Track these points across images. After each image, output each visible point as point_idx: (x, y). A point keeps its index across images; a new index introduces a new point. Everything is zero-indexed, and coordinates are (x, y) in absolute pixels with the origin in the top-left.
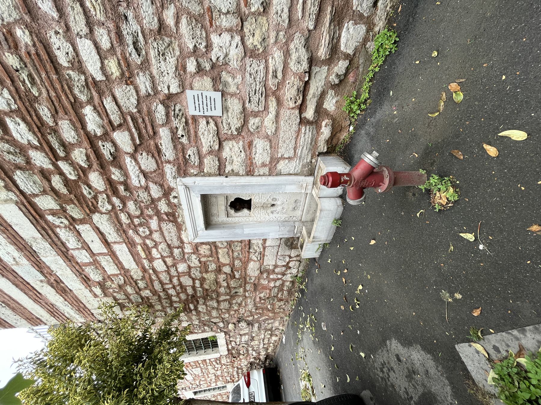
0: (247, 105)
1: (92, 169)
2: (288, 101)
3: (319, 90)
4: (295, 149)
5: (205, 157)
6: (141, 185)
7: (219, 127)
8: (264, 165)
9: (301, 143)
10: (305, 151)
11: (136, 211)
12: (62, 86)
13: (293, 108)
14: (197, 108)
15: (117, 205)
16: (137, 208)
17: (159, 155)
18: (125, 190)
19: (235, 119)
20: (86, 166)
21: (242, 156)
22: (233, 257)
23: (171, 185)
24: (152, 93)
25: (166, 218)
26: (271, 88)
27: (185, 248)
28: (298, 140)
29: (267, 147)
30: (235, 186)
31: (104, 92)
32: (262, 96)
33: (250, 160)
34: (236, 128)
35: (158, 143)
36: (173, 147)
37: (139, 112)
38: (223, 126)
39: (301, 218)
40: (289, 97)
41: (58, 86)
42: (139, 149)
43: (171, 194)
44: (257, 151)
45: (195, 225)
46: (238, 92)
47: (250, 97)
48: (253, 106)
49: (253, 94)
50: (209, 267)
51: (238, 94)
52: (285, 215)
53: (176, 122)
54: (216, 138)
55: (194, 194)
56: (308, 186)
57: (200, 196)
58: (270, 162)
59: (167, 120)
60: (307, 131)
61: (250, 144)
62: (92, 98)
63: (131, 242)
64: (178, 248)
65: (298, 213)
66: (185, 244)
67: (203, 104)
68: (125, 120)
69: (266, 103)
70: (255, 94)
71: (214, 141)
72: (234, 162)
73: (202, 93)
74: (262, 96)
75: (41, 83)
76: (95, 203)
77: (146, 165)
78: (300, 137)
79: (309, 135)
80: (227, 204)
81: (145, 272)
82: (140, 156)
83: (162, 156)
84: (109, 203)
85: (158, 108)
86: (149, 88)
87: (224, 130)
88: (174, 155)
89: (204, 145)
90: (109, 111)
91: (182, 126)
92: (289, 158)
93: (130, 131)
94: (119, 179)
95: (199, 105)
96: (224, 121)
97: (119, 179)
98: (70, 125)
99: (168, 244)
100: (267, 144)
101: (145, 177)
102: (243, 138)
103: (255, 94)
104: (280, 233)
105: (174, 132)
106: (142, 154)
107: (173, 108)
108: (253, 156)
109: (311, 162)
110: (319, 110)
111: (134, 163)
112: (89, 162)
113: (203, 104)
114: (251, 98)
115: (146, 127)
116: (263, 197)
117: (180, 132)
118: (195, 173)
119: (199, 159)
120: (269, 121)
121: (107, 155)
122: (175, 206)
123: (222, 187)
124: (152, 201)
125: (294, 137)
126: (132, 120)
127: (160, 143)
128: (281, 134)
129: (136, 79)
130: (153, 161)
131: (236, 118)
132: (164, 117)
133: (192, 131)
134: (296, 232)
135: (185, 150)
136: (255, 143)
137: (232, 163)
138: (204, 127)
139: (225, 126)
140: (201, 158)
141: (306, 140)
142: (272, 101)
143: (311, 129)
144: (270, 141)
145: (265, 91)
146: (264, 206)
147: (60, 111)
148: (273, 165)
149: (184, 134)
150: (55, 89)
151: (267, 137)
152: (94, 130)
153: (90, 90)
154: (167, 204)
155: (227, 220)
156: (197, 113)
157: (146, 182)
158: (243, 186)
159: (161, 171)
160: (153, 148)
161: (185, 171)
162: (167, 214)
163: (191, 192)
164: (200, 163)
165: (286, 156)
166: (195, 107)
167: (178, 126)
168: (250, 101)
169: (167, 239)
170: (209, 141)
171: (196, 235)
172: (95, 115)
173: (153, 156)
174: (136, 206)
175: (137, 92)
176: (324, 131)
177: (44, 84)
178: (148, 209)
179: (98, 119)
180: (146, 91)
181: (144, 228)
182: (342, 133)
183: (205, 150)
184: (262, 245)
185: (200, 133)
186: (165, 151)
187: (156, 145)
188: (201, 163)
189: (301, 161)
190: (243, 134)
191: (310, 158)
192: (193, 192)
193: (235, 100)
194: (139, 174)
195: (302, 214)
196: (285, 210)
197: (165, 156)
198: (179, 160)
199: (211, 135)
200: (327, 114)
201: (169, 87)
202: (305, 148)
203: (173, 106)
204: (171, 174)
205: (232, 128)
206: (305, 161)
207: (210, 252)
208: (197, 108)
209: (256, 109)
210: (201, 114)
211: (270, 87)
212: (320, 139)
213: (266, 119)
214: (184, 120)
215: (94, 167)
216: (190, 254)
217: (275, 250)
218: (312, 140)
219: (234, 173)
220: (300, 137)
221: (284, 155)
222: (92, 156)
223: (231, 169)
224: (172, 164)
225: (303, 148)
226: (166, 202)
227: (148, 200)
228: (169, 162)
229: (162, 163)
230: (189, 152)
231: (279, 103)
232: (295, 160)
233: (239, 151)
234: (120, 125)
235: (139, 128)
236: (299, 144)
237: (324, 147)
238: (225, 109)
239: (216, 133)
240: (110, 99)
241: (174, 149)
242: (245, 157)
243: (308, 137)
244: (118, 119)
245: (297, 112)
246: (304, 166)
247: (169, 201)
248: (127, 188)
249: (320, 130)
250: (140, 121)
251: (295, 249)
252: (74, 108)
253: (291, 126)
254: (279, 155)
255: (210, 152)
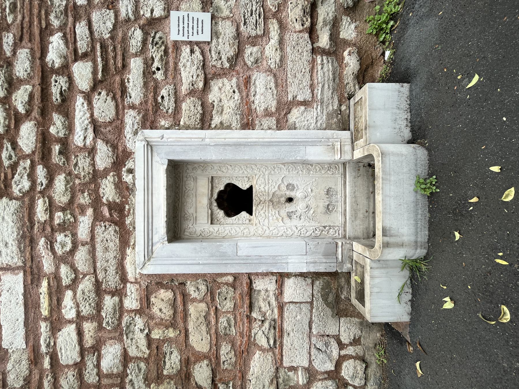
0: (242, 28)
1: (29, 118)
2: (293, 23)
3: (330, 15)
4: (312, 87)
5: (183, 100)
6: (84, 145)
7: (206, 57)
8: (268, 114)
9: (320, 78)
10: (328, 93)
11: (64, 195)
12: (40, 11)
13: (300, 32)
14: (181, 32)
15: (39, 181)
16: (66, 190)
17: (122, 96)
18: (60, 153)
19: (227, 44)
20: (23, 112)
21: (236, 98)
22: (216, 332)
23: (128, 146)
24: (132, 18)
25: (107, 214)
26: (270, 10)
27: (126, 295)
28: (315, 74)
29: (272, 84)
30: (225, 145)
31: (81, 17)
32: (260, 17)
33: (247, 105)
34: (228, 58)
35: (124, 79)
36: (142, 84)
37: (112, 38)
38: (211, 56)
39: (345, 231)
40: (293, 17)
41: (35, 11)
42: (99, 86)
43: (125, 165)
44: (258, 90)
45: (150, 232)
46: (232, 15)
47: (245, 20)
48: (249, 29)
49: (249, 15)
50: (164, 362)
51: (232, 17)
52: (313, 223)
53: (153, 50)
54: (200, 72)
55: (159, 159)
56: (344, 145)
57: (166, 162)
58: (278, 109)
59: (142, 48)
60: (325, 61)
61: (248, 81)
62: (65, 24)
63: (36, 271)
64: (113, 294)
65: (337, 219)
66: (128, 285)
67: (188, 27)
68: (93, 49)
69: (266, 26)
70: (251, 15)
71: (198, 76)
72: (225, 109)
73: (188, 14)
74: (260, 17)
75: (20, 9)
76: (9, 176)
77: (102, 110)
78: (316, 70)
79: (328, 67)
80: (212, 195)
81: (36, 364)
82: (97, 97)
83: (127, 97)
84: (28, 178)
85: (135, 33)
86: (130, 11)
87: (213, 61)
88: (142, 95)
89: (184, 81)
90: (78, 36)
91: (159, 56)
92: (305, 103)
93: (94, 62)
94: (58, 132)
95: (184, 27)
96: (213, 49)
97: (58, 132)
98: (29, 55)
99: (97, 281)
100: (271, 78)
101: (94, 132)
102: (238, 74)
103: (251, 15)
104: (310, 259)
105: (148, 63)
106: (100, 94)
107: (152, 35)
108: (252, 98)
109: (340, 111)
110: (334, 37)
111: (86, 107)
112: (29, 105)
113: (188, 27)
114: (247, 20)
115: (115, 58)
116: (270, 181)
117: (156, 64)
118: (166, 126)
119: (176, 102)
120: (271, 48)
121: (55, 91)
122: (127, 188)
123: (204, 147)
124: (94, 176)
125: (308, 70)
126: (101, 47)
127: (128, 79)
128: (290, 65)
129: (119, 3)
130: (112, 104)
131: (228, 43)
132: (139, 44)
133: (171, 64)
134: (340, 257)
135: (158, 90)
136: (253, 78)
137: (222, 113)
138: (187, 57)
139: (213, 56)
140: (178, 102)
141: (326, 74)
142: (273, 24)
143: (329, 59)
144: (275, 76)
145: (264, 11)
146: (275, 200)
147: (26, 37)
148: (283, 114)
149: (160, 67)
150: (31, 14)
151: (270, 70)
152: (53, 61)
153: (67, 16)
154: (115, 184)
155: (211, 229)
156: (180, 38)
157: (94, 139)
158: (237, 145)
159: (120, 122)
160: (117, 86)
161: (152, 122)
162: (111, 206)
163: (155, 154)
164: (175, 110)
165: (300, 98)
166: (179, 31)
167: (154, 56)
168: (245, 23)
169: (98, 265)
170: (191, 74)
171: (149, 255)
172: (61, 42)
173: (114, 98)
174: (66, 185)
175: (116, 16)
176: (349, 62)
177: (23, 11)
178: (83, 192)
179: (63, 46)
180: (126, 15)
181: (66, 236)
182: (376, 68)
183: (184, 89)
184: (277, 299)
185: (180, 65)
186: (132, 89)
187: (121, 80)
188: (177, 110)
189: (325, 107)
190: (237, 68)
191: (337, 102)
192: (158, 154)
193: (227, 23)
194: (87, 125)
195: (345, 222)
196: (312, 212)
197: (130, 97)
198: (147, 105)
199: (195, 67)
200: (346, 43)
201: (152, 11)
202: (326, 86)
203: (153, 33)
204: (131, 126)
205: (223, 57)
206: (331, 108)
207: (171, 312)
208: (181, 32)
209: (253, 33)
210: (185, 39)
211: (269, 8)
212: (345, 73)
213: (267, 47)
214: (163, 48)
215: (33, 114)
216: (133, 315)
217: (303, 317)
218: (334, 74)
219: (222, 126)
220: (316, 70)
221: (296, 96)
222: (37, 101)
223: (219, 121)
224: (137, 110)
225: (323, 86)
226: (114, 180)
227: (89, 173)
228: (133, 107)
229: (124, 107)
230: (164, 92)
231: (282, 27)
232: (315, 106)
233: (232, 91)
234: (85, 55)
235: (106, 59)
236: (316, 81)
237: (354, 86)
238: (215, 34)
239: (202, 64)
240: (83, 23)
241: (143, 87)
242: (239, 101)
243: (328, 70)
244: (85, 46)
245: (306, 35)
246: (330, 116)
247: (120, 177)
248: (64, 152)
249: (342, 62)
250: (111, 48)
251: (346, 316)
252: (42, 35)
253: (301, 54)
254: (290, 97)
255: (192, 93)
